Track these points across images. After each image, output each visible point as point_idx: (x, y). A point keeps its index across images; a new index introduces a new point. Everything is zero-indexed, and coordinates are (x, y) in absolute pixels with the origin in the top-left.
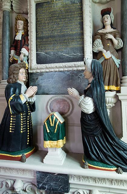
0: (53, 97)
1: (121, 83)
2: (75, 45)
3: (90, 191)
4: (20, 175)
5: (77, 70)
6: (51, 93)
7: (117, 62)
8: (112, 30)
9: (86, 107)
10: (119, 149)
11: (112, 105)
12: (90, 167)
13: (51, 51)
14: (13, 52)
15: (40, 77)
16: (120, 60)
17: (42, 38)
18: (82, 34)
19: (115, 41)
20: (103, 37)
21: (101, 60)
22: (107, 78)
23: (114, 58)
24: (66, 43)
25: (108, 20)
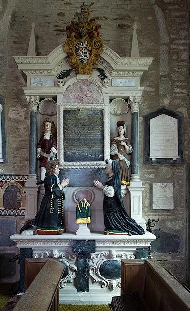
0: (78, 189)
1: (130, 179)
2: (97, 148)
3: (110, 251)
4: (57, 245)
5: (98, 168)
6: (76, 185)
7: (128, 163)
8: (125, 138)
9: (110, 192)
10: (130, 221)
11: (181, 89)
12: (110, 234)
13: (76, 151)
14: (39, 149)
15: (67, 173)
16: (43, 180)
17: (67, 140)
18: (103, 140)
19: (127, 147)
20: (118, 143)
21: (117, 161)
22: (121, 175)
23: (126, 160)
24: (90, 145)
25: (122, 130)
